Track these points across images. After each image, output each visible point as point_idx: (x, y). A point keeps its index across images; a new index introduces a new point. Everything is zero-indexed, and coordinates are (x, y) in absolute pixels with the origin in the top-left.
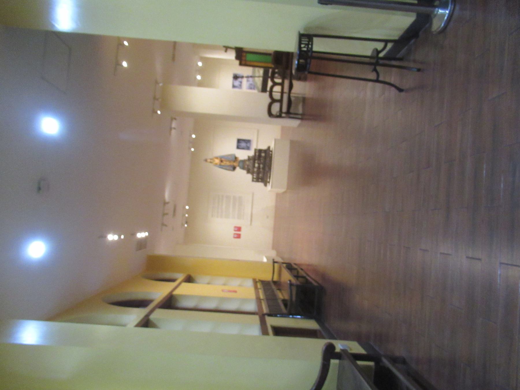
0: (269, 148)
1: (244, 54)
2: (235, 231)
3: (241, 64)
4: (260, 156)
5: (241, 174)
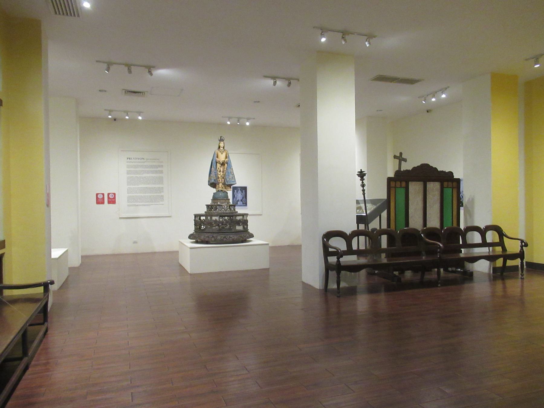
0: (252, 236)
1: (404, 184)
2: (109, 194)
3: (389, 180)
4: (238, 223)
5: (208, 194)
